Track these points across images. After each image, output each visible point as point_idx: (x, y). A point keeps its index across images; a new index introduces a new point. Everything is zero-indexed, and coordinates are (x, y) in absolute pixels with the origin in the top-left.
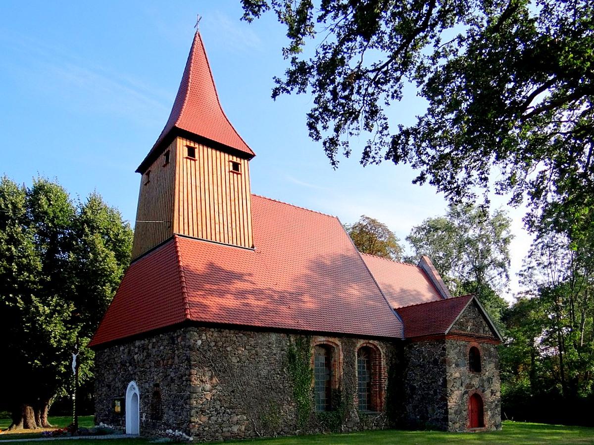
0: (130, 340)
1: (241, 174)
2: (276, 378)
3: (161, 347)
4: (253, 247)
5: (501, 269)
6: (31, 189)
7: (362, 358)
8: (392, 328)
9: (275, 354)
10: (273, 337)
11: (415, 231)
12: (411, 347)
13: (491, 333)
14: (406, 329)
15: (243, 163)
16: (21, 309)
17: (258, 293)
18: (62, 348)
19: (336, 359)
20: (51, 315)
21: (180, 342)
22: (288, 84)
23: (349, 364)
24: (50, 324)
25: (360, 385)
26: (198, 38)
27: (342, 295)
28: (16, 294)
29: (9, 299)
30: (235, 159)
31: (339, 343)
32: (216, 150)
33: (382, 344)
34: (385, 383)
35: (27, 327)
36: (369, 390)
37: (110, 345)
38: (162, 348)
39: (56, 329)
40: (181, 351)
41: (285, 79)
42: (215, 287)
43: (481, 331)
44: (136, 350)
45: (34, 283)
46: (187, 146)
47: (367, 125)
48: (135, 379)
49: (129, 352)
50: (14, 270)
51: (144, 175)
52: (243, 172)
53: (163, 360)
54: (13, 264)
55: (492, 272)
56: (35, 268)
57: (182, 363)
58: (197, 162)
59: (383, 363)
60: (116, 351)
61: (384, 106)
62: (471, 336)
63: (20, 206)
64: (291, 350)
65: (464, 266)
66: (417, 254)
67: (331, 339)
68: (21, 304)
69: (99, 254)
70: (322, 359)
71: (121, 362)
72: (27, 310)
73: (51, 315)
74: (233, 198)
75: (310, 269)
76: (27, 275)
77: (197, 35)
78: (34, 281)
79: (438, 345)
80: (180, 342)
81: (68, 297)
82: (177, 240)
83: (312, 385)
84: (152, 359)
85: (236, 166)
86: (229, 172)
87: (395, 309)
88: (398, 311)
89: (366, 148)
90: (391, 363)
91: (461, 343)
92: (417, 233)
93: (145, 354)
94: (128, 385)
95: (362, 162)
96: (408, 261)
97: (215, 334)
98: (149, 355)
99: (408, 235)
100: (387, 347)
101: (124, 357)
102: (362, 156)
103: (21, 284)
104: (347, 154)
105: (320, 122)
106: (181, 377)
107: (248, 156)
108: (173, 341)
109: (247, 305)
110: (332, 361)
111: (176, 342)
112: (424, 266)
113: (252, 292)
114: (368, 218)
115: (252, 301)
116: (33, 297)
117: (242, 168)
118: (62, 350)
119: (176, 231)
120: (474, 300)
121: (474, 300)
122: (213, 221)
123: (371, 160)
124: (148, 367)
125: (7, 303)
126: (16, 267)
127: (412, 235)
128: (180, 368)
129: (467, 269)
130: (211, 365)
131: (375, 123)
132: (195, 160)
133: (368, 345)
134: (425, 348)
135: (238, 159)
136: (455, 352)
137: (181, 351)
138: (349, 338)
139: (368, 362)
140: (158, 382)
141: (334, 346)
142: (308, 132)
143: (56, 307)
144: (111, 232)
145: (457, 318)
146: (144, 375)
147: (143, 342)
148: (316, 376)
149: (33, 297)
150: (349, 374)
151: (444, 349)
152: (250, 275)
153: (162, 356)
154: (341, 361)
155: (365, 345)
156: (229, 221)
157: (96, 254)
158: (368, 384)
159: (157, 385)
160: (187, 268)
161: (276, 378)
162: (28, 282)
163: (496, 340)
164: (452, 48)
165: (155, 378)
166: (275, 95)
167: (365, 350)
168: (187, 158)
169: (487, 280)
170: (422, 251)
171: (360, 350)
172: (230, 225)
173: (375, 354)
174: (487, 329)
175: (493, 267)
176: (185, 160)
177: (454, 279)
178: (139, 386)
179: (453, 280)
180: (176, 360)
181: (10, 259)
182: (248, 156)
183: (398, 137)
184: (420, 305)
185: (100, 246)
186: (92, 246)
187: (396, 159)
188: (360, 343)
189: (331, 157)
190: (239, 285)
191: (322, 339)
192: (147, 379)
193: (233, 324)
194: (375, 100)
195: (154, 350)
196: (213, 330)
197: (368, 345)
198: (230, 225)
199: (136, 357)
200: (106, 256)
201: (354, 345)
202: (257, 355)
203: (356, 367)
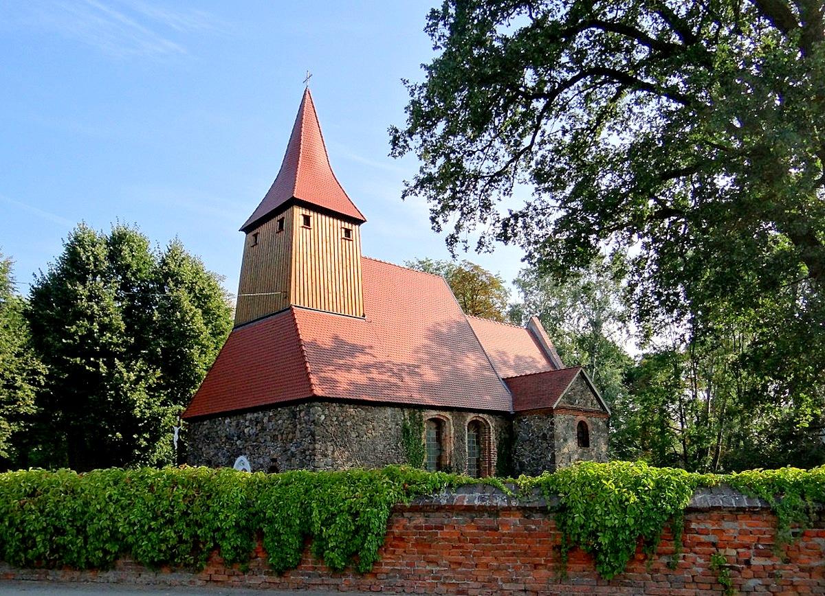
0: (242, 412)
1: (352, 241)
2: (390, 453)
3: (282, 419)
4: (364, 316)
5: (620, 324)
6: (109, 237)
7: (472, 432)
8: (501, 400)
9: (390, 429)
10: (389, 411)
11: (523, 273)
12: (520, 421)
13: (599, 406)
14: (515, 402)
15: (354, 228)
16: (104, 374)
17: (379, 366)
18: (145, 419)
19: (447, 433)
20: (137, 382)
21: (303, 417)
22: (416, 187)
23: (460, 438)
24: (135, 392)
25: (469, 460)
26: (307, 96)
27: (460, 366)
28: (97, 358)
29: (90, 364)
30: (347, 225)
31: (450, 417)
32: (333, 218)
33: (491, 417)
34: (495, 459)
35: (111, 395)
36: (478, 466)
37: (201, 419)
38: (280, 422)
39: (140, 397)
40: (304, 425)
41: (413, 183)
42: (341, 362)
43: (589, 404)
44: (247, 424)
45: (117, 345)
46: (303, 215)
47: (481, 217)
48: (245, 454)
49: (237, 425)
50: (95, 330)
51: (251, 234)
52: (354, 239)
53: (282, 434)
54: (94, 324)
55: (610, 327)
56: (118, 328)
57: (305, 437)
58: (312, 231)
59: (493, 438)
60: (220, 424)
61: (496, 202)
62: (579, 410)
63: (102, 258)
64: (405, 426)
65: (579, 319)
66: (525, 301)
67: (442, 413)
68: (103, 370)
69: (187, 313)
70: (433, 434)
71: (226, 436)
72: (110, 375)
73: (137, 382)
74: (344, 266)
75: (428, 338)
76: (110, 336)
77: (307, 93)
78: (117, 343)
79: (546, 419)
80: (303, 417)
81: (151, 360)
82: (294, 311)
83: (425, 460)
84: (268, 433)
85: (348, 232)
86: (342, 238)
87: (503, 379)
88: (508, 381)
89: (481, 237)
90: (500, 437)
91: (569, 417)
92: (526, 276)
93: (259, 427)
94: (235, 460)
95: (476, 250)
96: (515, 315)
97: (337, 409)
98: (263, 429)
99: (515, 278)
100: (496, 421)
101: (232, 430)
102: (477, 245)
103: (104, 346)
104: (466, 248)
105: (441, 216)
106: (304, 452)
107: (358, 222)
108: (294, 415)
109: (371, 379)
110: (443, 436)
111: (298, 417)
112: (533, 328)
113: (374, 366)
114: (471, 264)
115: (375, 374)
116: (117, 361)
117: (353, 234)
118: (146, 421)
119: (292, 302)
120: (581, 373)
121: (581, 373)
122: (326, 291)
123: (484, 249)
124: (262, 441)
125: (87, 368)
126: (98, 327)
127: (520, 277)
128: (303, 442)
129: (583, 322)
130: (333, 440)
131: (488, 217)
132: (310, 229)
133: (375, 374)
134: (535, 423)
135: (350, 225)
136: (563, 424)
137: (304, 425)
138: (459, 411)
139: (478, 437)
140: (275, 457)
141: (444, 420)
142: (431, 225)
143: (140, 372)
144: (197, 287)
145: (565, 392)
146: (257, 449)
147: (256, 415)
148: (427, 450)
149: (117, 361)
150: (459, 449)
151: (552, 424)
152: (371, 347)
153: (280, 430)
154: (452, 436)
155: (475, 419)
156: (342, 290)
157: (184, 313)
158: (478, 460)
159: (274, 460)
160: (313, 344)
161: (390, 453)
162: (111, 344)
163: (604, 414)
164: (556, 137)
165: (272, 452)
166: (403, 197)
167: (475, 425)
168: (303, 227)
169: (605, 336)
170: (532, 298)
171: (469, 424)
172: (342, 294)
173: (485, 428)
174: (595, 402)
175: (612, 321)
176: (301, 229)
177: (569, 333)
178: (250, 461)
179: (568, 334)
180: (298, 434)
181: (91, 318)
182: (358, 222)
183: (509, 220)
184: (530, 375)
185: (186, 304)
186: (176, 305)
187: (507, 239)
188: (470, 417)
189: (452, 252)
190: (362, 359)
191: (433, 414)
192: (261, 453)
193: (360, 400)
194: (489, 195)
195: (270, 424)
196: (334, 404)
197: (478, 418)
198: (342, 294)
199: (246, 430)
200: (194, 315)
201: (464, 418)
202: (374, 430)
203: (466, 442)
